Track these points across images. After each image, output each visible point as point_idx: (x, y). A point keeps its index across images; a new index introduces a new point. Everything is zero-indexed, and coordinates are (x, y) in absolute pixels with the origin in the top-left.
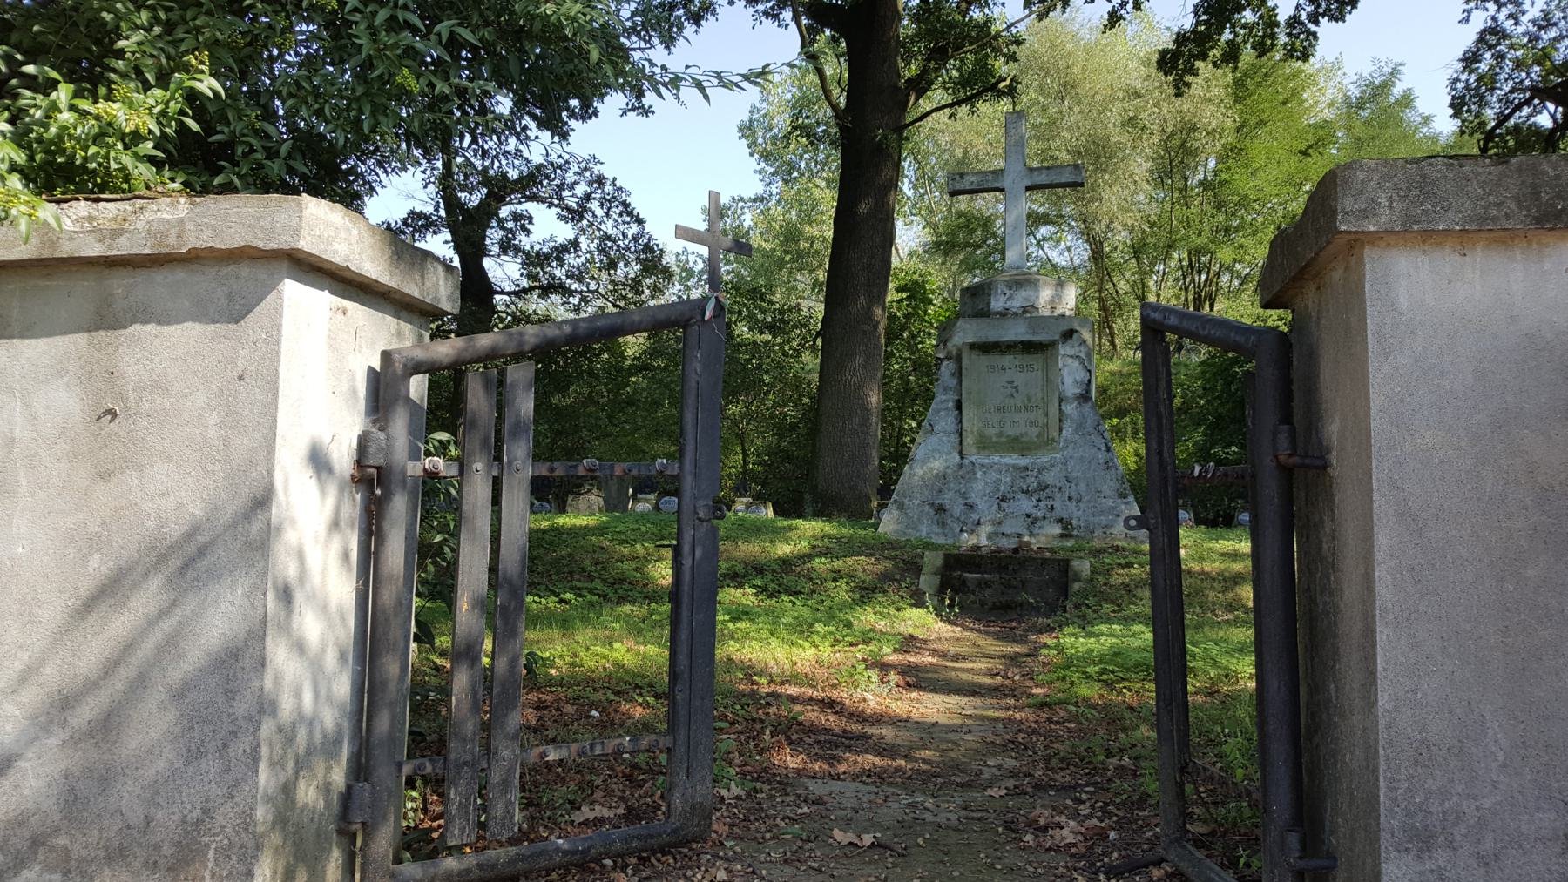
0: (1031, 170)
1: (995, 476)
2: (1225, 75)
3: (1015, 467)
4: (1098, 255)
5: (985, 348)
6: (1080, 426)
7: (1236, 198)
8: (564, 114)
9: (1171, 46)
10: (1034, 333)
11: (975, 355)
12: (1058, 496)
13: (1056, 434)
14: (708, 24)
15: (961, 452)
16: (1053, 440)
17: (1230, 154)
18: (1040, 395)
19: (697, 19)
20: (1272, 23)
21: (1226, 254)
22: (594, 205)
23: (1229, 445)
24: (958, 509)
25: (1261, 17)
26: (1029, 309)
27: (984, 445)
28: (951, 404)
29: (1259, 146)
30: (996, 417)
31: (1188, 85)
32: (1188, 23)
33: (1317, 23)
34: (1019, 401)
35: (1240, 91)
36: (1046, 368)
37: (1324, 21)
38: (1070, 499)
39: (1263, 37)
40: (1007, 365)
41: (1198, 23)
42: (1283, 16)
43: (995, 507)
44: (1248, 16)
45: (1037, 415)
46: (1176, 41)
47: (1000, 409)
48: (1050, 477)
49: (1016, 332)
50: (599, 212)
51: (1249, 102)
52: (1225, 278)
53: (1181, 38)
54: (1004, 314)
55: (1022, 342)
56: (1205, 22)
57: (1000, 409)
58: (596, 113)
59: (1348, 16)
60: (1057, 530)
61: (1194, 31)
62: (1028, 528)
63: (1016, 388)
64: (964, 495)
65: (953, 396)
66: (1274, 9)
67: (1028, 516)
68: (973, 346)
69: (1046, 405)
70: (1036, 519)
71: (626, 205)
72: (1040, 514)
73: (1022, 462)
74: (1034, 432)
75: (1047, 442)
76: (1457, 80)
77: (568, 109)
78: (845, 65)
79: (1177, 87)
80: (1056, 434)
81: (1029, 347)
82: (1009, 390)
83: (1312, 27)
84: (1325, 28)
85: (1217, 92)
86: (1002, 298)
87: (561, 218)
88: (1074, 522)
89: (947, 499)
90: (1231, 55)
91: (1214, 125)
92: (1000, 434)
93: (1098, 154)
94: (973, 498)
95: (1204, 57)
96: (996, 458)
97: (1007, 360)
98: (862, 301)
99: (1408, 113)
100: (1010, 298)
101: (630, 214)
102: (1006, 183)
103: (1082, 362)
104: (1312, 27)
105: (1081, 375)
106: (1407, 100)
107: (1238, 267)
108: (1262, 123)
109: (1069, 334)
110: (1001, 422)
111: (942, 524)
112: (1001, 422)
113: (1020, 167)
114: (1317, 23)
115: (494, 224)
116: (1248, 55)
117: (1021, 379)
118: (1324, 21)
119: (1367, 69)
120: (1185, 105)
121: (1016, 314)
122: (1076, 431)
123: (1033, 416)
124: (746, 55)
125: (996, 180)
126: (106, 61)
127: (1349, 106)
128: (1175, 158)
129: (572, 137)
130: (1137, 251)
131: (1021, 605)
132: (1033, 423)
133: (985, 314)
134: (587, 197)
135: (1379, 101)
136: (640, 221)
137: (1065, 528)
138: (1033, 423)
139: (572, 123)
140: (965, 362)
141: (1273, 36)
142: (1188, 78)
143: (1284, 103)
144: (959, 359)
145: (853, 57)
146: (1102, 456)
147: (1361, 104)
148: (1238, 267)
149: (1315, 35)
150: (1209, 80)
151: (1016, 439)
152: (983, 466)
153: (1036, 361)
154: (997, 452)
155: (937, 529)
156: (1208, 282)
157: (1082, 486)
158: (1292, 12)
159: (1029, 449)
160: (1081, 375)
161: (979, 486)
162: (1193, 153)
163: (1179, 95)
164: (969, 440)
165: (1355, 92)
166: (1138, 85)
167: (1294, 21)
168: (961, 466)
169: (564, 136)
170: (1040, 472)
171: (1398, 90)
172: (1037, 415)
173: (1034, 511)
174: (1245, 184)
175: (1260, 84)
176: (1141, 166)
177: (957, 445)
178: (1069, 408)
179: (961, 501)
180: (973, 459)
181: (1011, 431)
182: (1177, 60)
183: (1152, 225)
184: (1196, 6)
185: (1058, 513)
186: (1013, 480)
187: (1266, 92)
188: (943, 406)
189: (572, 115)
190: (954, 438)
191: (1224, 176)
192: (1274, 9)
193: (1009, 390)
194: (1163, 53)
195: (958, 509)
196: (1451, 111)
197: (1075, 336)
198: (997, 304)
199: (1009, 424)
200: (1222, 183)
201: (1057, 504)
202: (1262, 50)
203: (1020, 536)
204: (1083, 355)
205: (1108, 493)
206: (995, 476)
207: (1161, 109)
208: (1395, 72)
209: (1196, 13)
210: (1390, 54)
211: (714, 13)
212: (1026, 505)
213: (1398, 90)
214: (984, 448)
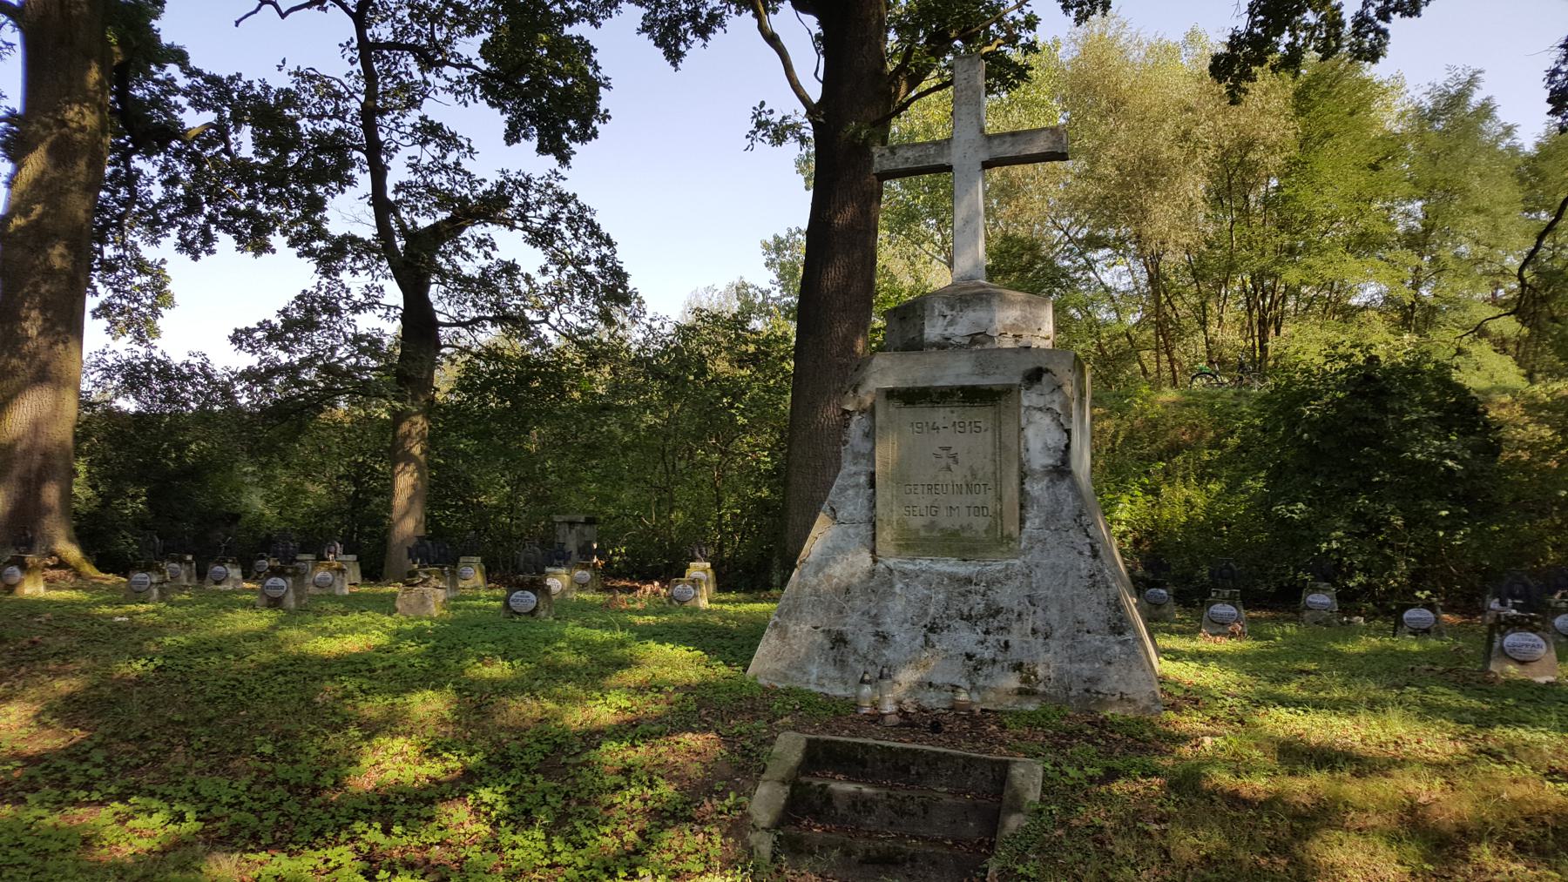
0: (990, 138)
1: (922, 590)
2: (1287, 85)
3: (953, 578)
4: (1155, 279)
5: (908, 397)
6: (1052, 516)
7: (1300, 216)
8: (565, 136)
9: (1223, 49)
10: (984, 374)
11: (893, 407)
12: (1016, 626)
13: (1013, 529)
14: (717, 37)
15: (873, 552)
16: (1010, 538)
17: (1292, 168)
18: (990, 468)
19: (703, 31)
20: (1335, 23)
21: (1292, 275)
22: (562, 226)
23: (1294, 501)
24: (864, 642)
25: (1323, 18)
26: (978, 338)
27: (911, 544)
28: (863, 479)
29: (1324, 162)
31: (1246, 91)
32: (1242, 24)
33: (1387, 19)
34: (959, 475)
35: (1302, 102)
36: (998, 427)
37: (1396, 17)
38: (1034, 631)
39: (1327, 38)
40: (940, 423)
41: (1254, 24)
42: (1348, 15)
43: (920, 640)
44: (1310, 17)
45: (987, 498)
46: (1230, 45)
47: (931, 488)
48: (1006, 596)
49: (957, 372)
50: (568, 234)
51: (1312, 114)
52: (1291, 304)
53: (1235, 42)
54: (944, 345)
55: (962, 388)
56: (1262, 23)
57: (931, 488)
58: (595, 134)
59: (1424, 10)
60: (1012, 681)
61: (1250, 33)
62: (969, 677)
63: (954, 457)
64: (875, 620)
65: (863, 466)
66: (1338, 7)
67: (969, 657)
68: (890, 394)
69: (998, 482)
70: (982, 662)
71: (591, 223)
72: (988, 655)
73: (963, 570)
74: (980, 524)
75: (1001, 541)
76: (1555, 72)
77: (568, 129)
78: (822, 60)
79: (1231, 94)
80: (1013, 529)
81: (973, 396)
83: (1383, 25)
84: (1397, 25)
85: (1276, 103)
86: (941, 322)
87: (528, 241)
88: (1041, 671)
89: (851, 624)
90: (1292, 60)
91: (1274, 136)
92: (931, 526)
93: (1149, 173)
94: (889, 625)
95: (1261, 61)
96: (924, 563)
97: (941, 415)
98: (841, 330)
99: (1488, 125)
100: (952, 323)
101: (600, 237)
102: (954, 157)
103: (1056, 417)
104: (1383, 25)
105: (1055, 438)
106: (1486, 110)
107: (1304, 290)
108: (1328, 135)
109: (1035, 376)
110: (933, 509)
111: (841, 663)
113: (972, 133)
114: (1387, 19)
116: (1311, 56)
117: (960, 443)
118: (1396, 17)
119: (1441, 78)
120: (1240, 117)
121: (960, 346)
122: (1046, 524)
124: (763, 67)
125: (940, 154)
127: (1421, 118)
128: (1232, 177)
129: (573, 160)
130: (1198, 272)
131: (913, 858)
132: (979, 510)
133: (915, 345)
134: (554, 218)
135: (1456, 116)
136: (609, 243)
137: (1025, 680)
138: (979, 510)
139: (573, 145)
140: (880, 417)
141: (1338, 36)
142: (1244, 84)
143: (1352, 114)
144: (871, 412)
145: (829, 44)
146: (1085, 565)
147: (1434, 115)
148: (1304, 290)
149: (1385, 33)
150: (1268, 92)
151: (955, 534)
152: (904, 574)
153: (982, 415)
154: (925, 553)
155: (833, 672)
156: (1274, 304)
157: (1054, 613)
158: (1359, 8)
159: (975, 550)
160: (1055, 438)
161: (897, 605)
162: (1250, 168)
163: (1235, 101)
164: (886, 535)
165: (1428, 103)
166: (1192, 102)
167: (1361, 21)
168: (872, 573)
169: (564, 159)
170: (988, 587)
171: (1476, 99)
172: (987, 498)
173: (978, 650)
174: (1308, 198)
175: (1323, 95)
176: (1195, 186)
177: (868, 542)
178: (1036, 488)
179: (870, 628)
180: (891, 562)
181: (946, 521)
182: (1233, 66)
183: (1210, 246)
184: (1251, 5)
185: (1014, 655)
186: (948, 599)
187: (1330, 103)
188: (852, 481)
189: (573, 138)
190: (865, 530)
191: (1286, 191)
192: (1338, 7)
193: (943, 462)
194: (1216, 58)
195: (864, 642)
196: (1550, 107)
197: (1045, 378)
198: (933, 330)
199: (944, 512)
200: (1285, 200)
201: (1014, 639)
202: (1327, 52)
203: (955, 688)
204: (1057, 407)
205: (1094, 625)
206: (922, 590)
207: (1217, 125)
208: (1472, 81)
209: (1251, 12)
210: (1465, 62)
211: (722, 25)
212: (966, 638)
213: (1476, 99)
214: (908, 547)
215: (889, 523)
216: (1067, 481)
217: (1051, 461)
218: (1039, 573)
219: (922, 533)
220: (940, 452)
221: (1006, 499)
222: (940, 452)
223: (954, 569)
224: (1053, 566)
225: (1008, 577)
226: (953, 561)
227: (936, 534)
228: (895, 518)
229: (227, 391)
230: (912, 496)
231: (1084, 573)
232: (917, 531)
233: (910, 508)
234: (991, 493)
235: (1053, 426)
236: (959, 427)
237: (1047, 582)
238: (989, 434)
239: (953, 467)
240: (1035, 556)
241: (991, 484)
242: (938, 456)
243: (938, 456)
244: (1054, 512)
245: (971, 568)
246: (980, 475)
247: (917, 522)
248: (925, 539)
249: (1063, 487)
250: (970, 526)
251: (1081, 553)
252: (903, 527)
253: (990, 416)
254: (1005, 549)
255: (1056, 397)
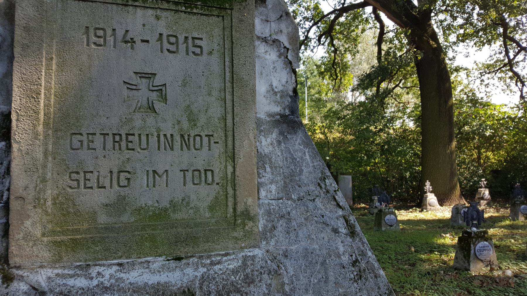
18: (216, 111)
30: (107, 162)
40: (136, 33)
45: (209, 156)
57: (120, 140)
63: (161, 92)
74: (203, 195)
82: (143, 94)
92: (118, 205)
110: (123, 175)
112: (123, 175)
115: (345, 6)
117: (170, 69)
122: (286, 191)
123: (200, 159)
126: (329, 38)
132: (202, 175)
138: (202, 175)
151: (160, 215)
154: (109, 254)
159: (192, 240)
172: (209, 156)
181: (146, 195)
193: (143, 94)
199: (141, 180)
214: (75, 245)
215: (38, 202)
216: (300, 134)
217: (277, 109)
218: (290, 267)
219: (103, 219)
220: (135, 80)
221: (240, 161)
222: (135, 80)
223: (163, 278)
224: (307, 253)
225: (249, 280)
226: (158, 262)
227: (127, 218)
228: (49, 193)
229: (93, 215)
230: (84, 154)
231: (345, 259)
232: (93, 215)
233: (79, 174)
234: (218, 149)
235: (280, 64)
236: (170, 43)
237: (303, 280)
238: (215, 61)
239: (158, 106)
240: (279, 242)
241: (219, 135)
242: (130, 86)
243: (130, 86)
244: (292, 176)
245: (189, 271)
246: (202, 120)
247: (94, 199)
248: (108, 229)
249: (296, 142)
250: (186, 201)
251: (336, 231)
252: (66, 210)
253: (217, 31)
254: (239, 233)
255: (283, 26)
